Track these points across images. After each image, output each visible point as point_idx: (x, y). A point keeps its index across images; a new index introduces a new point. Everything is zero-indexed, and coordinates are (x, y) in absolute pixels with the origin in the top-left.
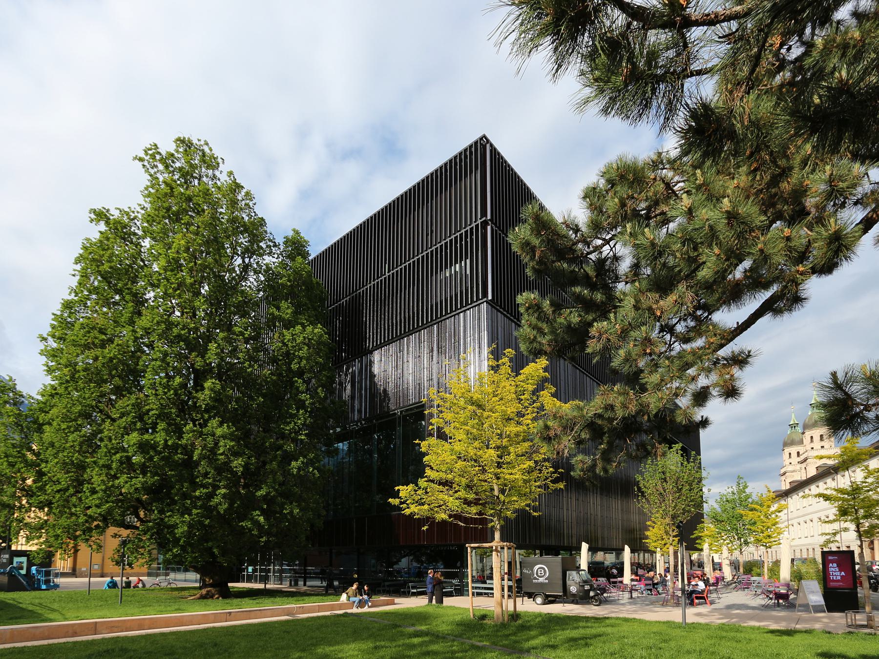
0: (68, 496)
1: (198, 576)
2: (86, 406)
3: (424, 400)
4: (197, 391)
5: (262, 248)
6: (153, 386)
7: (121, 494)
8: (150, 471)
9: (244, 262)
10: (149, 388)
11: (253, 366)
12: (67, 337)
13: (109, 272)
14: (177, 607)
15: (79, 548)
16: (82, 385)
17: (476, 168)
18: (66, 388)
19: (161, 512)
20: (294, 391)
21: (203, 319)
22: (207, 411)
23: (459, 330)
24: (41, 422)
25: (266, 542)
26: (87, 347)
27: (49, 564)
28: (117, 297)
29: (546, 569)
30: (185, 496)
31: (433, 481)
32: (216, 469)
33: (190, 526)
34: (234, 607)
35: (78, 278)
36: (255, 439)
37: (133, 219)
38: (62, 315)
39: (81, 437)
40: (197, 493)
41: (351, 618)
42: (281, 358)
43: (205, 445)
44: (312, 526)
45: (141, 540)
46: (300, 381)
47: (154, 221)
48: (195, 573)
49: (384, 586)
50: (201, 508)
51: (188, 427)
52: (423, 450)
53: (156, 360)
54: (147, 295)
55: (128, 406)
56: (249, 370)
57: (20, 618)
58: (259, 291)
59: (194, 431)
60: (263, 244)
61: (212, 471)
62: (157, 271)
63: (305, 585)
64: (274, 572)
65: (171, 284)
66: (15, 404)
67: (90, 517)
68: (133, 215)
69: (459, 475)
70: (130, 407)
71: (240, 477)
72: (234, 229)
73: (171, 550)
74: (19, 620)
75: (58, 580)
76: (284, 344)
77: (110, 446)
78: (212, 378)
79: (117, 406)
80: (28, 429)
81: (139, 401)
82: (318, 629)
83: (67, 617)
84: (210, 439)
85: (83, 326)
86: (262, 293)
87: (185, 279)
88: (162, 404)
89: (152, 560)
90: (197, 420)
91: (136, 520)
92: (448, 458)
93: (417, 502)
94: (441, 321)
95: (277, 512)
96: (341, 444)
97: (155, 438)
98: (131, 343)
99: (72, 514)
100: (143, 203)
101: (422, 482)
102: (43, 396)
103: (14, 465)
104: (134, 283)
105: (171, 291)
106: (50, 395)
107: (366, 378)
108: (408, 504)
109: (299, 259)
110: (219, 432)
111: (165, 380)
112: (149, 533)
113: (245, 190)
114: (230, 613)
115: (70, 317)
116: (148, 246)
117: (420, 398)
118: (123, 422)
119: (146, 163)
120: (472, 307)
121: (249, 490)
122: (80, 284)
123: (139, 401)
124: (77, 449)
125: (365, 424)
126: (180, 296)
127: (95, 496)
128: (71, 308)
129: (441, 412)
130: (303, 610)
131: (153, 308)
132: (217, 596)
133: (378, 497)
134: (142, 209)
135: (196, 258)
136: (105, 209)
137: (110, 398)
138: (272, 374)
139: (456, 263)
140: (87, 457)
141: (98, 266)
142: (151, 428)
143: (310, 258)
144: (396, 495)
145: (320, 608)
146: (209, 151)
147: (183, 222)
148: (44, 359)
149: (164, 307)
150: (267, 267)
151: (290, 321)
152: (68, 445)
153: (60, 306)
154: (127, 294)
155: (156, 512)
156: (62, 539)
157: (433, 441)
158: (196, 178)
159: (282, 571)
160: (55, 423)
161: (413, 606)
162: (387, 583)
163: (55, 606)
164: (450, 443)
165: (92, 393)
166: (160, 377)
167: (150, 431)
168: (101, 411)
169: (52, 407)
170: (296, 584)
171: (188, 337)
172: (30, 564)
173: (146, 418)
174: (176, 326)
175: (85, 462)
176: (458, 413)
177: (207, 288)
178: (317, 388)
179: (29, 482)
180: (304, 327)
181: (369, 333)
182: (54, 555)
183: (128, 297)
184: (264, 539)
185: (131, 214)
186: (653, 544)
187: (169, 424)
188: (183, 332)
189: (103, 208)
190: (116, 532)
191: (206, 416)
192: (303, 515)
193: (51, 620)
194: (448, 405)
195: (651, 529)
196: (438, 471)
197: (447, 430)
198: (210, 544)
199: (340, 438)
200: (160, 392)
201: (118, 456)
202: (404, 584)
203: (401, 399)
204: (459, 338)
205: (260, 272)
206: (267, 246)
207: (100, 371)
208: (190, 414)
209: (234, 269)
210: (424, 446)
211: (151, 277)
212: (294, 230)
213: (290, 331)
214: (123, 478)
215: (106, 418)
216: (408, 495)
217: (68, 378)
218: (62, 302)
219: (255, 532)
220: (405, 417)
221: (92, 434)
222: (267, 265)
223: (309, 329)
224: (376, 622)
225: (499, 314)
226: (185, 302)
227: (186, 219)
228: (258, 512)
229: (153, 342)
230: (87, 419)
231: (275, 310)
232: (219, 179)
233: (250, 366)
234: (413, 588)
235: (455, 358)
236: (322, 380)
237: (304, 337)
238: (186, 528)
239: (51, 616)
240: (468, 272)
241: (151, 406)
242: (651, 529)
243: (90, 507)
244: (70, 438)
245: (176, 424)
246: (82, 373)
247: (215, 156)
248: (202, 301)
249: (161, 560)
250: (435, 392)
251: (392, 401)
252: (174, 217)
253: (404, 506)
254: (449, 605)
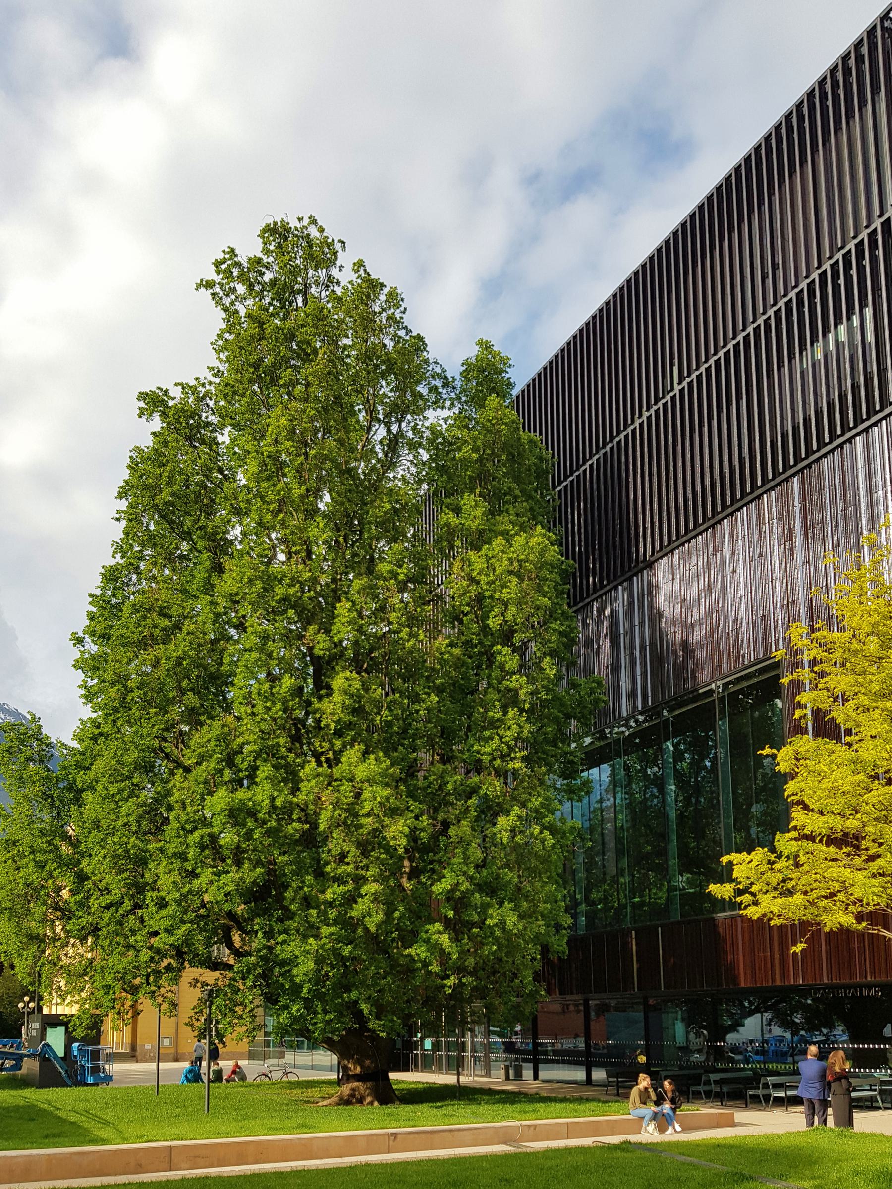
0: (123, 916)
1: (335, 1058)
2: (144, 751)
3: (779, 654)
4: (320, 698)
5: (421, 396)
6: (248, 701)
7: (203, 905)
8: (249, 859)
9: (389, 431)
10: (241, 703)
11: (415, 636)
12: (112, 632)
13: (172, 504)
14: (300, 1121)
15: (140, 1007)
16: (138, 714)
17: (875, 90)
18: (114, 721)
19: (269, 935)
20: (496, 673)
21: (325, 560)
22: (339, 733)
23: (855, 479)
24: (80, 786)
25: (455, 987)
26: (143, 644)
27: (96, 1040)
28: (185, 546)
30: (308, 902)
31: (811, 838)
32: (359, 844)
33: (320, 961)
34: (402, 1124)
35: (124, 523)
36: (425, 778)
37: (203, 398)
38: (103, 595)
39: (139, 806)
40: (328, 895)
41: (638, 1153)
42: (468, 609)
43: (338, 799)
44: (545, 950)
45: (236, 991)
46: (506, 650)
47: (234, 393)
48: (329, 1053)
49: (708, 1083)
50: (336, 922)
51: (307, 769)
52: (783, 767)
53: (250, 650)
54: (232, 533)
55: (209, 741)
56: (409, 644)
57: (59, 1136)
58: (420, 482)
59: (318, 775)
60: (422, 389)
61: (353, 849)
62: (244, 486)
63: (536, 1077)
64: (474, 1050)
65: (269, 504)
66: (41, 762)
67: (158, 951)
68: (203, 390)
69: (876, 819)
70: (213, 743)
71: (401, 858)
72: (368, 373)
73: (286, 1007)
74: (57, 1140)
75: (114, 1068)
76: (473, 581)
77: (184, 818)
78: (344, 669)
79: (192, 743)
80: (61, 801)
81: (226, 729)
82: (568, 1176)
83: (127, 1135)
84: (346, 787)
85: (135, 609)
86: (425, 486)
87: (290, 490)
88: (262, 732)
89: (259, 1028)
90: (322, 753)
91: (227, 951)
92: (846, 779)
93: (775, 889)
94: (809, 466)
95: (473, 925)
96: (595, 771)
97: (254, 795)
98: (209, 626)
99: (129, 947)
100: (216, 363)
101: (785, 842)
102: (81, 740)
103: (43, 867)
104: (209, 514)
105: (269, 517)
106: (91, 739)
107: (642, 624)
108: (753, 894)
109: (493, 400)
110: (361, 772)
111: (266, 686)
112: (251, 977)
113: (386, 291)
114: (395, 1135)
115: (114, 596)
116: (228, 442)
117: (766, 647)
118: (201, 772)
119: (217, 289)
121: (419, 883)
122: (127, 533)
123: (226, 729)
124: (134, 829)
125: (645, 721)
126: (283, 524)
127: (164, 912)
128: (116, 580)
129: (822, 675)
130: (538, 1134)
131: (241, 554)
132: (369, 1099)
133: (681, 881)
134: (215, 375)
135: (306, 445)
136: (161, 390)
137: (181, 731)
138: (451, 644)
139: (838, 322)
140: (148, 842)
141: (153, 498)
142: (248, 777)
143: (515, 392)
144: (725, 875)
145: (571, 1131)
146: (318, 235)
147: (282, 382)
148: (80, 675)
149: (258, 550)
150: (433, 433)
151: (481, 533)
152: (120, 823)
153: (100, 578)
154: (200, 537)
155: (260, 935)
156: (114, 993)
157: (805, 743)
158: (299, 292)
159: (489, 1048)
160: (99, 787)
161: (781, 1131)
162: (713, 1077)
163: (109, 1115)
164: (850, 745)
165: (154, 725)
166: (258, 680)
167: (245, 782)
168: (167, 756)
169: (94, 758)
170: (519, 1075)
171: (300, 598)
172: (70, 1040)
173: (238, 759)
174: (280, 581)
175: (147, 851)
176: (864, 672)
177: (327, 498)
178: (541, 660)
179: (65, 893)
180: (509, 540)
181: (645, 524)
182: (102, 1021)
183: (201, 544)
184: (452, 981)
185: (200, 389)
187: (276, 767)
188: (292, 591)
189: (159, 388)
190: (196, 976)
191: (338, 743)
192: (525, 928)
193: (103, 1142)
194: (837, 656)
196: (821, 813)
197: (839, 715)
198: (354, 995)
199: (594, 758)
200: (259, 709)
201: (197, 834)
202: (755, 1080)
203: (724, 657)
204: (856, 496)
205: (420, 445)
206: (430, 390)
207: (163, 684)
208: (309, 744)
209: (372, 450)
210: (784, 759)
211: (235, 499)
212: (480, 343)
213: (483, 552)
214: (206, 875)
215: (176, 768)
216: (752, 873)
217: (116, 703)
218: (103, 571)
219: (435, 968)
220: (733, 696)
221: (156, 800)
222: (432, 428)
223: (519, 540)
224: (696, 1167)
226: (292, 533)
227: (287, 375)
228: (438, 926)
229: (244, 617)
230: (147, 772)
231: (451, 515)
232: (338, 283)
233: (411, 635)
234: (777, 1086)
235: (848, 542)
236: (549, 641)
237: (510, 560)
238: (311, 965)
239: (102, 1133)
240: (870, 337)
241: (246, 737)
243: (156, 934)
244: (123, 810)
245: (287, 766)
246: (136, 693)
247: (330, 240)
248: (321, 525)
249: (270, 1029)
250: (805, 630)
251: (705, 663)
252: (268, 378)
253: (746, 898)
254: (868, 1129)
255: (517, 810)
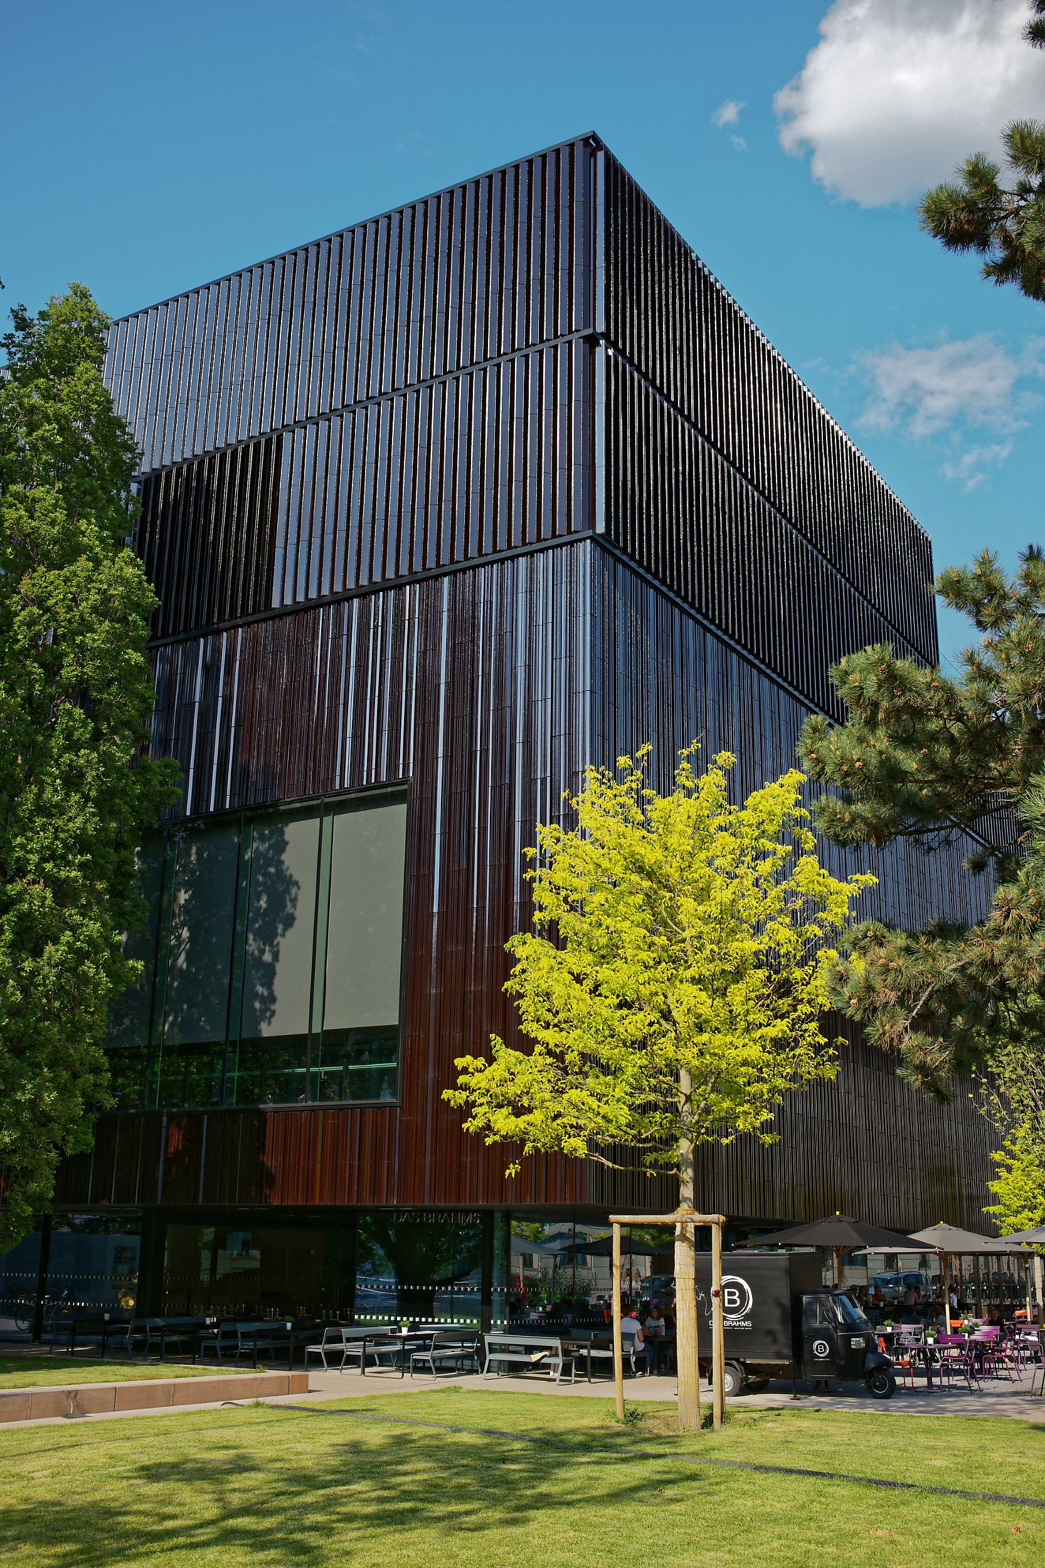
29: (746, 1286)
120: (553, 548)
186: (1012, 1220)
195: (1003, 1173)
212: (988, 274)
225: (782, 692)
242: (1003, 1173)
255: (67, 936)
